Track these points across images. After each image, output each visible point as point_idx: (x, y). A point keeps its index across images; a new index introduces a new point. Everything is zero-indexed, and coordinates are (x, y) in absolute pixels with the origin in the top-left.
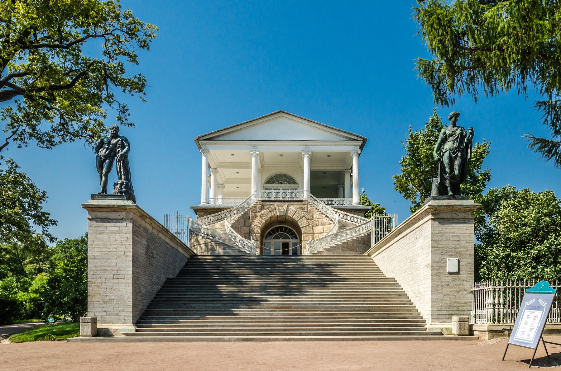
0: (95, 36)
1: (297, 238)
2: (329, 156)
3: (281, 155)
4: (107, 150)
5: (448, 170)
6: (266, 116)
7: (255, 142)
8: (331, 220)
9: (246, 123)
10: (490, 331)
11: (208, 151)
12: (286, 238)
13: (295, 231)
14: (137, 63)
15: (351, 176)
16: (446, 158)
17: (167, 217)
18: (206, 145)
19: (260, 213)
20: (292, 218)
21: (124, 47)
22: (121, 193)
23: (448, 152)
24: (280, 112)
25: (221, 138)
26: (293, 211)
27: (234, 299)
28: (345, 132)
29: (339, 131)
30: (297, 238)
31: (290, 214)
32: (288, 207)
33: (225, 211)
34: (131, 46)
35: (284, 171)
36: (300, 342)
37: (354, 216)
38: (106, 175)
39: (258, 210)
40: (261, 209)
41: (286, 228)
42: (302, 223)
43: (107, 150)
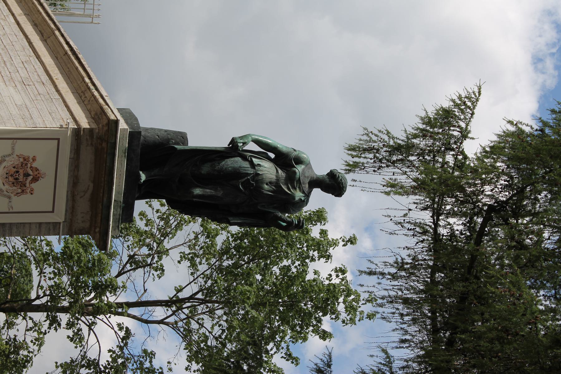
5: (206, 169)
16: (236, 165)
23: (251, 171)
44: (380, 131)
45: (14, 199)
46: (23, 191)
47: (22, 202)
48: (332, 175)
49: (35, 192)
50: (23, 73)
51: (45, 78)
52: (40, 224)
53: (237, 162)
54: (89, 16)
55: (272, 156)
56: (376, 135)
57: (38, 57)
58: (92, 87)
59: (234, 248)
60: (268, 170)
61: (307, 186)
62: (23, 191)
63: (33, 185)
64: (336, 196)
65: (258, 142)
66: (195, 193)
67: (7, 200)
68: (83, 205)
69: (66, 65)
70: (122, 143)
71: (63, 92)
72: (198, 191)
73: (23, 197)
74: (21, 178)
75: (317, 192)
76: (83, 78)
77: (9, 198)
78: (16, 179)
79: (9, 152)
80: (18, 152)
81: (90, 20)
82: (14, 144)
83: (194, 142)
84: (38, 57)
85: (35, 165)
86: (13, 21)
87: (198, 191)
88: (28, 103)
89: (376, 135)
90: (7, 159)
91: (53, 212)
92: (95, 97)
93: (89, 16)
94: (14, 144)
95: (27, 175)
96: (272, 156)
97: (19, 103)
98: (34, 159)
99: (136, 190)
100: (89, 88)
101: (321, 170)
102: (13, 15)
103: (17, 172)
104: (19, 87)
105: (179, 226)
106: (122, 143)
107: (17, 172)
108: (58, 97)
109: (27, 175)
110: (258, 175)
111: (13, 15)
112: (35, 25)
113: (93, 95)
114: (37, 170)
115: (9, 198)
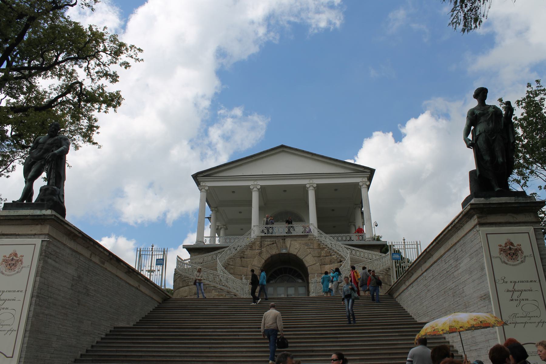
5: (487, 158)
15: (362, 213)
17: (140, 251)
21: (107, 69)
23: (484, 135)
31: (293, 251)
39: (257, 248)
44: (452, 16)
45: (23, 265)
46: (520, 250)
47: (527, 249)
48: (476, 96)
49: (519, 243)
50: (452, 261)
51: (452, 250)
52: (537, 239)
53: (481, 140)
54: (417, 246)
55: (472, 128)
56: (454, 19)
57: (442, 256)
58: (453, 224)
60: (481, 128)
62: (520, 250)
63: (515, 245)
64: (487, 92)
65: (467, 134)
67: (527, 258)
68: (521, 218)
70: (482, 200)
71: (458, 239)
72: (500, 160)
73: (523, 249)
74: (513, 251)
75: (488, 102)
76: (449, 230)
77: (525, 257)
78: (514, 254)
79: (499, 259)
80: (498, 255)
81: (419, 246)
82: (494, 257)
83: (474, 167)
84: (442, 256)
85: (504, 245)
86: (425, 273)
87: (500, 160)
88: (468, 255)
89: (454, 19)
91: (528, 233)
92: (459, 221)
93: (417, 246)
94: (494, 257)
96: (472, 128)
97: (469, 259)
98: (500, 246)
99: (506, 191)
100: (454, 226)
101: (474, 103)
102: (422, 274)
103: (509, 254)
104: (459, 262)
105: (452, 330)
106: (482, 200)
107: (509, 254)
108: (462, 241)
110: (485, 131)
111: (422, 274)
113: (458, 222)
114: (506, 244)
115: (525, 257)
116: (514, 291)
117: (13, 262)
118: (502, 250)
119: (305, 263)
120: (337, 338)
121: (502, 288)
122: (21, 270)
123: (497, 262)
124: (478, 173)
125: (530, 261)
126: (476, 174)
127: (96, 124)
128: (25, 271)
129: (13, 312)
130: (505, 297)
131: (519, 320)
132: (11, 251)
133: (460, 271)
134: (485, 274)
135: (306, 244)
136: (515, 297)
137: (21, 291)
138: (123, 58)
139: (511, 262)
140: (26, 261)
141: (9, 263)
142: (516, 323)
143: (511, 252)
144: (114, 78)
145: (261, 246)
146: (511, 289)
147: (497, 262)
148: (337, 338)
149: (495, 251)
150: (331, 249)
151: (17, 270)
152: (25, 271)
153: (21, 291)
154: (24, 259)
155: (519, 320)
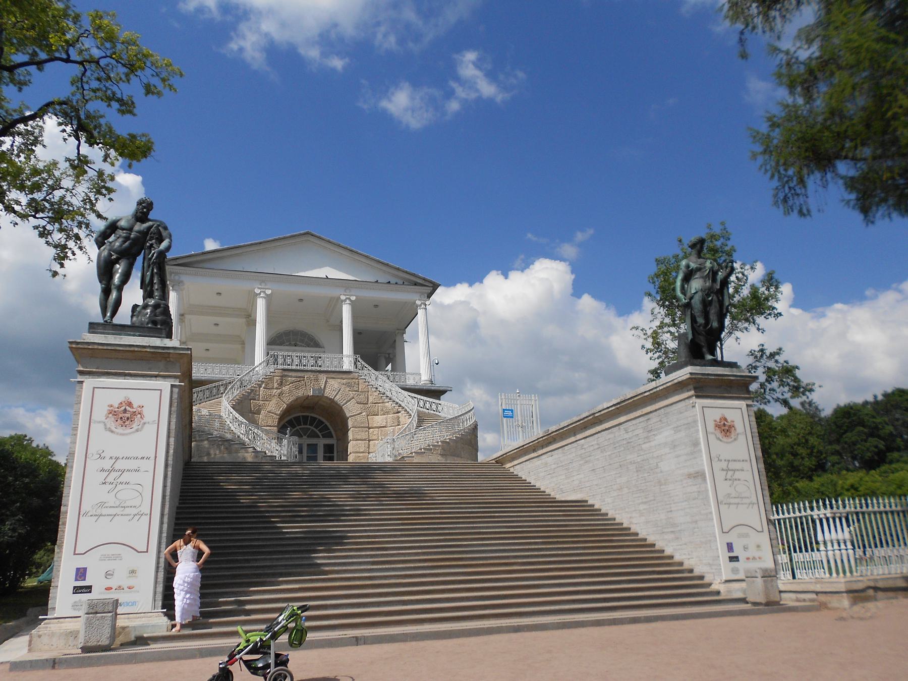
0: (68, 60)
1: (332, 437)
2: (376, 306)
3: (301, 300)
4: (124, 242)
6: (285, 238)
7: (263, 277)
8: (400, 406)
9: (252, 245)
10: (849, 592)
11: (180, 283)
12: (314, 435)
13: (328, 424)
14: (134, 115)
16: (698, 303)
18: (176, 274)
19: (279, 391)
20: (332, 400)
21: (115, 88)
22: (155, 323)
23: (700, 294)
24: (307, 233)
25: (201, 265)
26: (333, 389)
27: (901, 538)
28: (406, 272)
29: (398, 269)
30: (332, 437)
31: (329, 393)
32: (326, 382)
33: (210, 386)
34: (132, 89)
35: (301, 326)
36: (514, 636)
37: (431, 400)
38: (120, 289)
39: (276, 385)
40: (281, 384)
41: (314, 419)
42: (350, 409)
43: (124, 242)
45: (145, 420)
49: (141, 405)
59: (6, 180)
61: (787, 440)
63: (135, 406)
66: (139, 179)
69: (854, 549)
73: (736, 426)
74: (727, 428)
79: (102, 425)
82: (95, 422)
90: (108, 426)
94: (95, 422)
95: (125, 411)
109: (125, 411)
112: (543, 447)
116: (728, 470)
117: (128, 415)
118: (717, 426)
119: (346, 411)
120: (494, 517)
121: (717, 466)
122: (142, 427)
123: (712, 438)
124: (690, 337)
125: (742, 438)
126: (687, 338)
127: (109, 184)
128: (150, 430)
129: (139, 488)
130: (720, 476)
131: (733, 501)
132: (122, 399)
133: (652, 444)
134: (700, 451)
135: (348, 385)
136: (729, 477)
137: (148, 458)
138: (146, 75)
139: (725, 439)
140: (150, 414)
141: (121, 415)
142: (730, 504)
143: (725, 428)
144: (126, 107)
145: (281, 384)
146: (725, 468)
147: (712, 438)
148: (494, 517)
149: (711, 427)
150: (384, 394)
151: (135, 426)
152: (150, 430)
153: (148, 458)
154: (145, 411)
155: (733, 501)
